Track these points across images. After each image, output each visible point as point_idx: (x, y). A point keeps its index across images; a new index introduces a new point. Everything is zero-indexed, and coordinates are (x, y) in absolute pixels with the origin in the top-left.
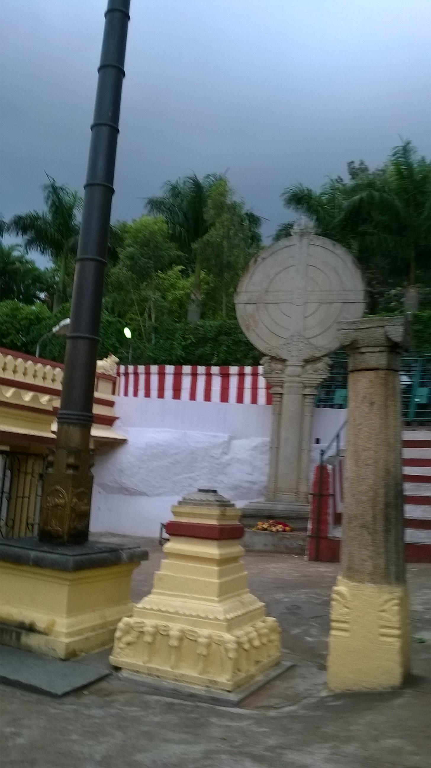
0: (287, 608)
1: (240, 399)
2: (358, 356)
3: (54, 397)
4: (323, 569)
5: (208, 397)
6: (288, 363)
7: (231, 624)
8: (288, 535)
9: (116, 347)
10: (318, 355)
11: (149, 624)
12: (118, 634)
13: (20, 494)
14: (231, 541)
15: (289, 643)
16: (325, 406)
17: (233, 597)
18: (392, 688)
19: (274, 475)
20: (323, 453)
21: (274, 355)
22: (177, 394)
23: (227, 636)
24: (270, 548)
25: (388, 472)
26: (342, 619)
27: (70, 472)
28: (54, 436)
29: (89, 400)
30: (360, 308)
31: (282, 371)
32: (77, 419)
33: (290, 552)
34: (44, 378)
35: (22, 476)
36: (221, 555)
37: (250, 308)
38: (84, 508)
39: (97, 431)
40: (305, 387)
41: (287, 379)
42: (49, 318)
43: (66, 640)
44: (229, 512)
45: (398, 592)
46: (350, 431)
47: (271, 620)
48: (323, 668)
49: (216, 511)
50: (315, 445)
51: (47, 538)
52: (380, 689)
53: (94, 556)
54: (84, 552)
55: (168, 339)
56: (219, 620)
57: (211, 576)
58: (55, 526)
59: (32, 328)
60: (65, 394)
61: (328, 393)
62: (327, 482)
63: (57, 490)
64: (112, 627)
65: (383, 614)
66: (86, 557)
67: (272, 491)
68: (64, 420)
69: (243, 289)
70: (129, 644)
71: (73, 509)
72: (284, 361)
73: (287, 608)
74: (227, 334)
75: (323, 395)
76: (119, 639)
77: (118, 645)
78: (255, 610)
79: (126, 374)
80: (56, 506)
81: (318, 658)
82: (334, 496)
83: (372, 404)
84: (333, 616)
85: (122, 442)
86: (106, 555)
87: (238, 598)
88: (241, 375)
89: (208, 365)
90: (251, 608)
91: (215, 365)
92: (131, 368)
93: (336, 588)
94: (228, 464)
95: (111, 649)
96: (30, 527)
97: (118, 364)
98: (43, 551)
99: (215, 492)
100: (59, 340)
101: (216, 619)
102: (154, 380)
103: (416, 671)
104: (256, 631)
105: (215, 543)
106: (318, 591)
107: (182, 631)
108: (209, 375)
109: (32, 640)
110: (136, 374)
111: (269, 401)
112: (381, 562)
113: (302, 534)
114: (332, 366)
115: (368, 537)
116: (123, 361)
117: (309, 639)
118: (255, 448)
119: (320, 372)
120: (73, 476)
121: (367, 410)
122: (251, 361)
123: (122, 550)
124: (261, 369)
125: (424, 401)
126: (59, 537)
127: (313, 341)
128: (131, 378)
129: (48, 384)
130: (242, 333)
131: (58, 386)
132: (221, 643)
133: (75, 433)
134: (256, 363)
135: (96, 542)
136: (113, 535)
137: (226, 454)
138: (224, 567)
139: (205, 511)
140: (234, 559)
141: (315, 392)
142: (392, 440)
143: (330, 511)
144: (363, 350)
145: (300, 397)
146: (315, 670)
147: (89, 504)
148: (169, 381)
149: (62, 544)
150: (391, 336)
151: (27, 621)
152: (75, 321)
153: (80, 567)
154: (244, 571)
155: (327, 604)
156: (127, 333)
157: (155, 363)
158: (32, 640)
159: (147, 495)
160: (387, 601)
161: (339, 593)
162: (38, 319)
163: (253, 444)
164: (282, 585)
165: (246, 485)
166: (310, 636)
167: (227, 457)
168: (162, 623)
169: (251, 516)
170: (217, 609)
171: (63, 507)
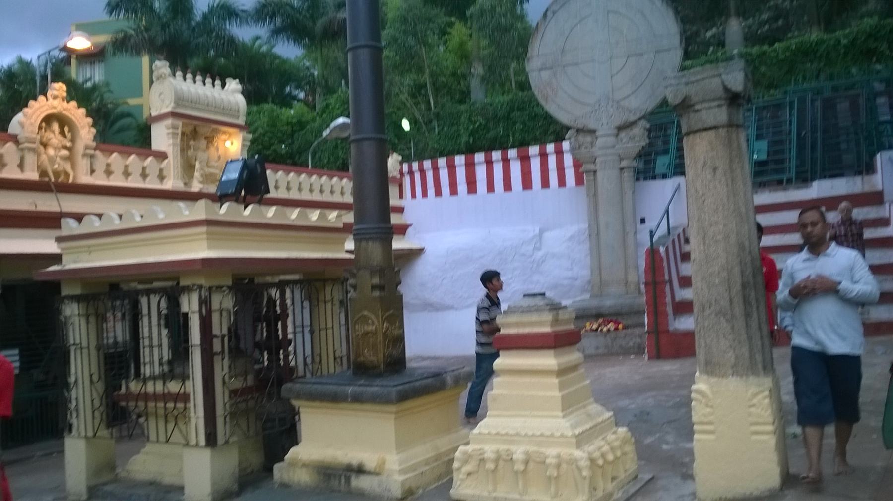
0: (635, 416)
1: (545, 184)
2: (692, 115)
3: (343, 212)
4: (669, 367)
5: (508, 186)
6: (598, 134)
7: (581, 440)
8: (622, 333)
9: (395, 144)
10: (632, 118)
11: (489, 450)
12: (456, 465)
13: (323, 325)
14: (567, 349)
15: (645, 454)
16: (645, 179)
17: (577, 410)
18: (770, 490)
19: (598, 267)
20: (652, 234)
21: (580, 126)
22: (472, 188)
23: (578, 454)
24: (601, 351)
25: (741, 247)
26: (706, 420)
27: (376, 294)
28: (352, 256)
29: (385, 209)
30: (677, 55)
31: (592, 144)
32: (376, 233)
33: (625, 352)
34: (288, 189)
35: (322, 305)
36: (559, 365)
37: (545, 75)
38: (397, 332)
39: (398, 244)
40: (621, 159)
41: (599, 152)
42: (314, 120)
43: (401, 478)
44: (562, 315)
45: (768, 382)
46: (699, 204)
47: (622, 430)
48: (688, 476)
49: (548, 317)
50: (639, 226)
51: (362, 370)
52: (756, 493)
53: (417, 384)
54: (406, 380)
55: (453, 125)
56: (566, 437)
57: (551, 389)
58: (369, 356)
59: (296, 135)
60: (358, 206)
61: (647, 162)
62: (662, 268)
63: (364, 316)
64: (447, 459)
65: (752, 410)
66: (407, 386)
67: (598, 286)
68: (362, 236)
69: (535, 52)
70: (469, 474)
71: (385, 335)
72: (593, 132)
73: (635, 416)
74: (521, 109)
75: (641, 166)
76: (459, 469)
77: (458, 477)
78: (602, 422)
79: (411, 173)
80: (366, 334)
81: (682, 465)
82: (670, 281)
83: (715, 170)
84: (695, 418)
85: (420, 251)
86: (429, 380)
87: (583, 411)
88: (544, 156)
89: (504, 148)
90: (600, 420)
91: (513, 147)
92: (415, 165)
93: (694, 387)
94: (543, 261)
95: (452, 480)
96: (339, 360)
97: (401, 163)
98: (360, 385)
99: (543, 294)
100: (341, 143)
101: (562, 436)
102: (444, 174)
103: (793, 470)
104: (609, 444)
105: (551, 352)
106: (667, 392)
107: (527, 453)
108: (506, 161)
109: (361, 483)
110: (422, 171)
111: (579, 181)
112: (745, 350)
113: (637, 331)
114: (650, 131)
115: (724, 324)
116: (406, 159)
117: (665, 447)
118: (571, 238)
119: (637, 139)
120: (380, 298)
121: (709, 177)
122: (552, 137)
123: (446, 372)
124: (566, 145)
125: (764, 157)
126: (375, 367)
127: (622, 103)
128: (417, 176)
129: (337, 198)
130: (538, 104)
131: (349, 199)
132: (572, 462)
133: (375, 250)
134: (559, 139)
135: (415, 369)
136: (424, 359)
137: (539, 249)
138: (564, 378)
139: (534, 317)
140: (574, 368)
141: (635, 164)
142: (743, 210)
143: (668, 299)
144: (697, 107)
145: (616, 172)
146: (678, 480)
147: (402, 326)
148: (461, 173)
149: (380, 375)
150: (729, 86)
151: (355, 463)
152: (357, 121)
153: (404, 397)
154: (584, 381)
155: (687, 403)
156: (406, 125)
157: (442, 155)
158: (361, 483)
159: (457, 309)
160: (756, 395)
161: (698, 392)
162: (300, 125)
163: (569, 235)
164: (626, 391)
165: (566, 282)
166: (667, 443)
167: (540, 254)
168: (503, 447)
169: (583, 316)
170: (560, 425)
171: (375, 333)
